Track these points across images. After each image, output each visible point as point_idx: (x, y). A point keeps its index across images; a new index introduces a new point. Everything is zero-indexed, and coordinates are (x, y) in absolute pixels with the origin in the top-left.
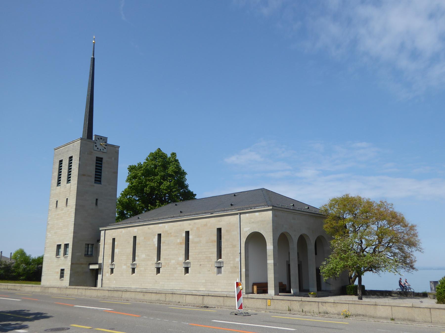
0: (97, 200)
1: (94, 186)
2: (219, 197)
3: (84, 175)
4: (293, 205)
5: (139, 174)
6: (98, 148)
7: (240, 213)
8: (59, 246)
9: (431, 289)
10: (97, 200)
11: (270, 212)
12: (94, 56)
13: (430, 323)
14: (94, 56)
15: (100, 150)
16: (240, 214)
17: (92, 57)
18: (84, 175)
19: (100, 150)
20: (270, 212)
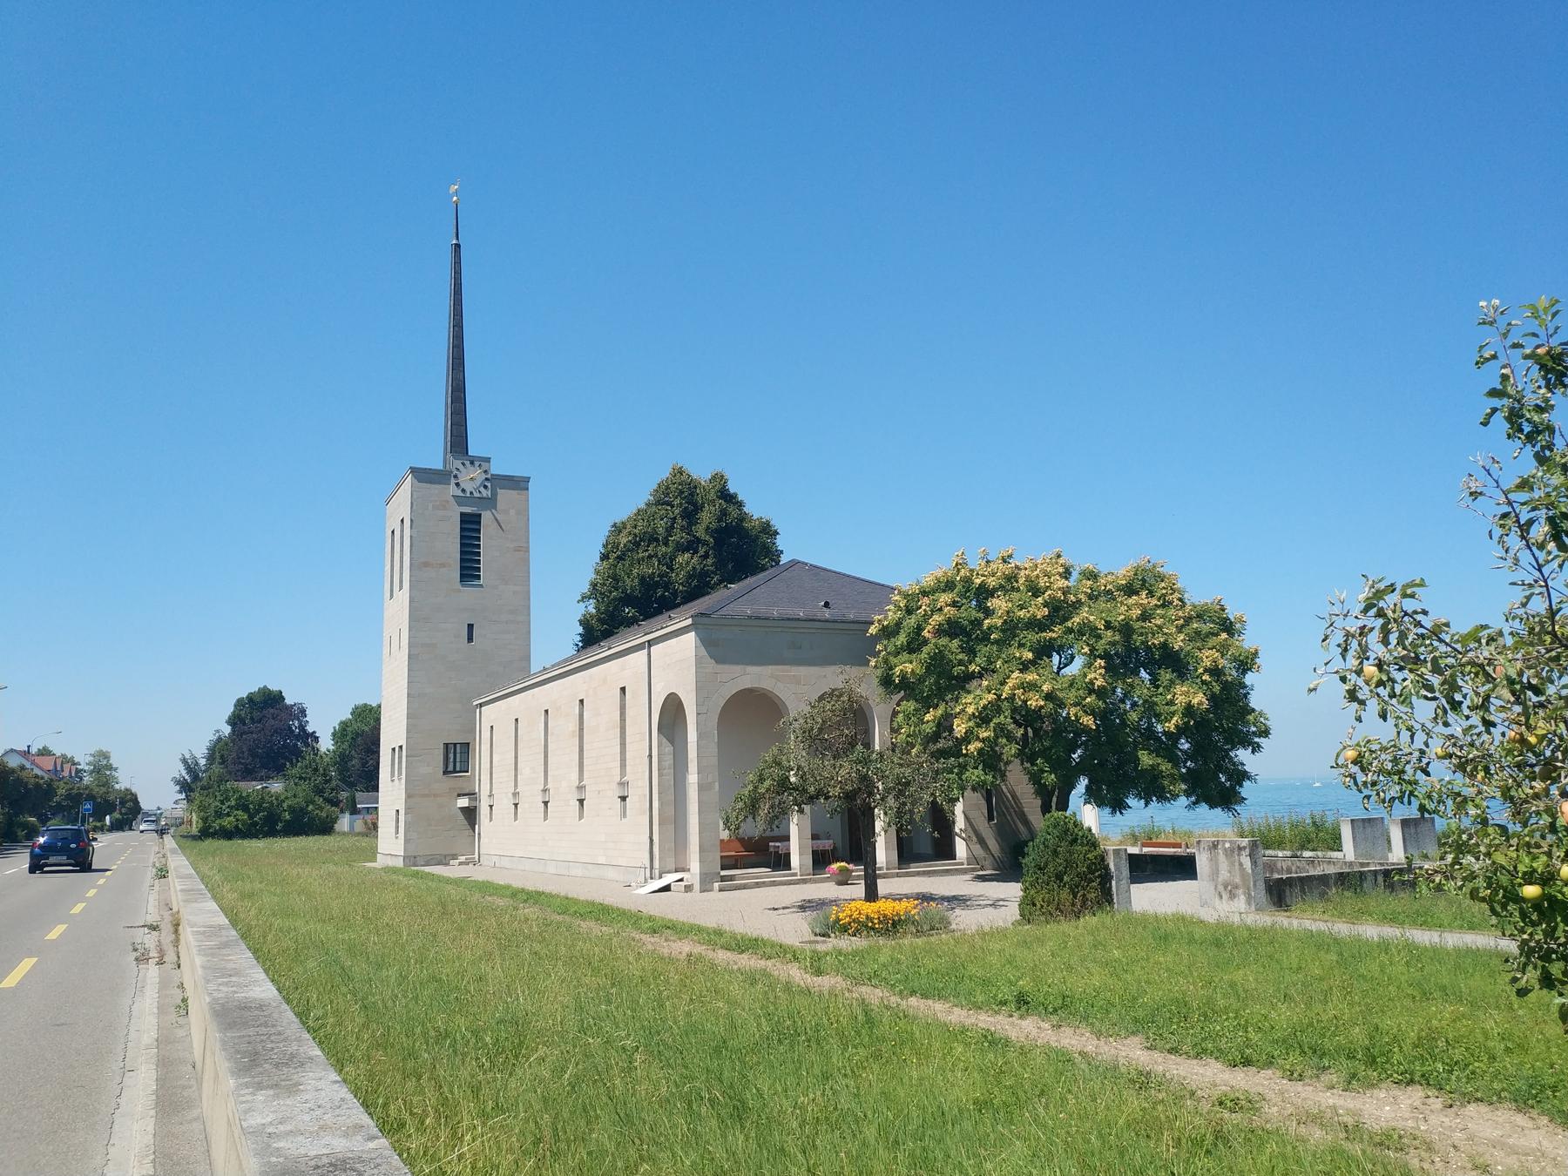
0: (470, 627)
1: (460, 591)
2: (414, 548)
3: (426, 564)
4: (827, 605)
5: (1100, 674)
6: (463, 491)
7: (649, 641)
8: (394, 749)
9: (1236, 756)
10: (470, 627)
11: (691, 637)
12: (457, 239)
13: (1289, 882)
14: (457, 239)
15: (471, 493)
16: (650, 643)
17: (454, 242)
18: (426, 564)
19: (471, 493)
20: (691, 637)
